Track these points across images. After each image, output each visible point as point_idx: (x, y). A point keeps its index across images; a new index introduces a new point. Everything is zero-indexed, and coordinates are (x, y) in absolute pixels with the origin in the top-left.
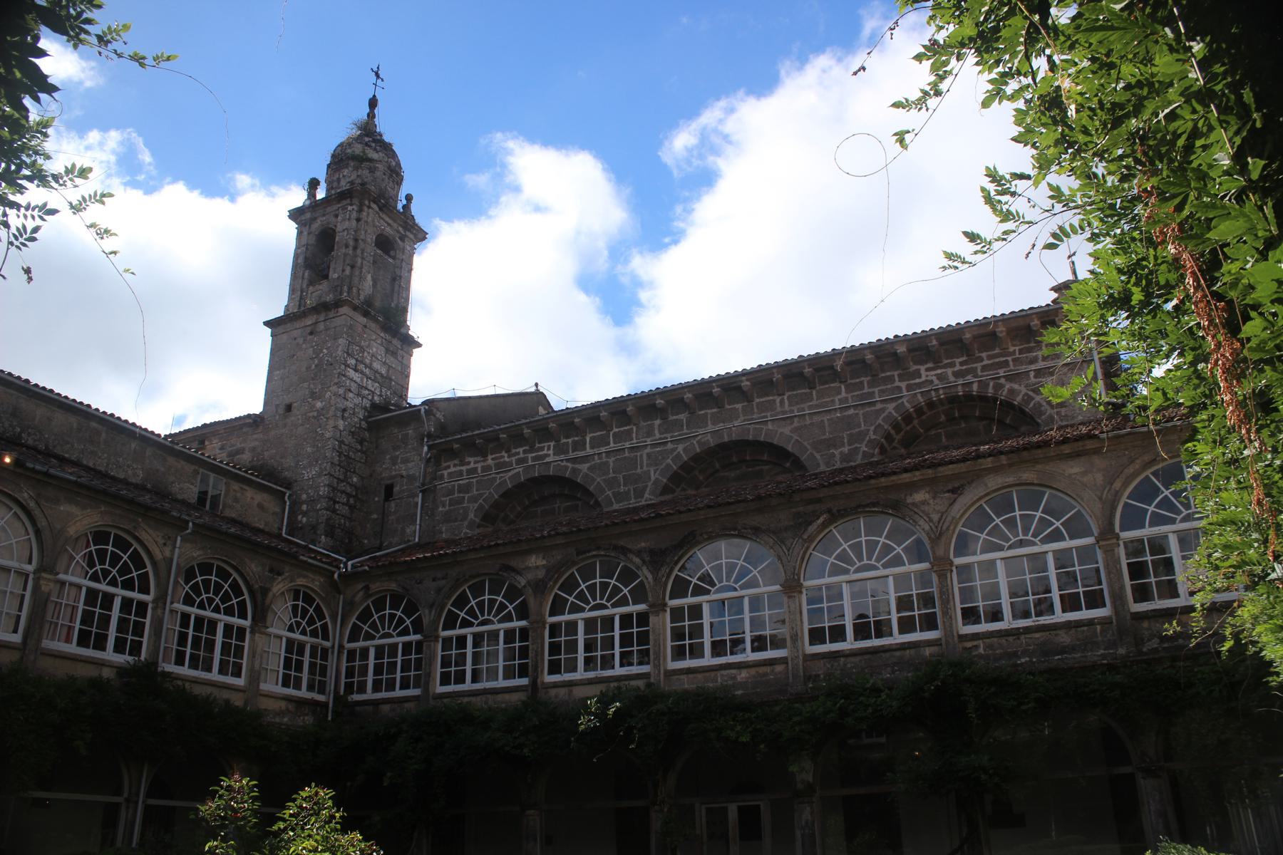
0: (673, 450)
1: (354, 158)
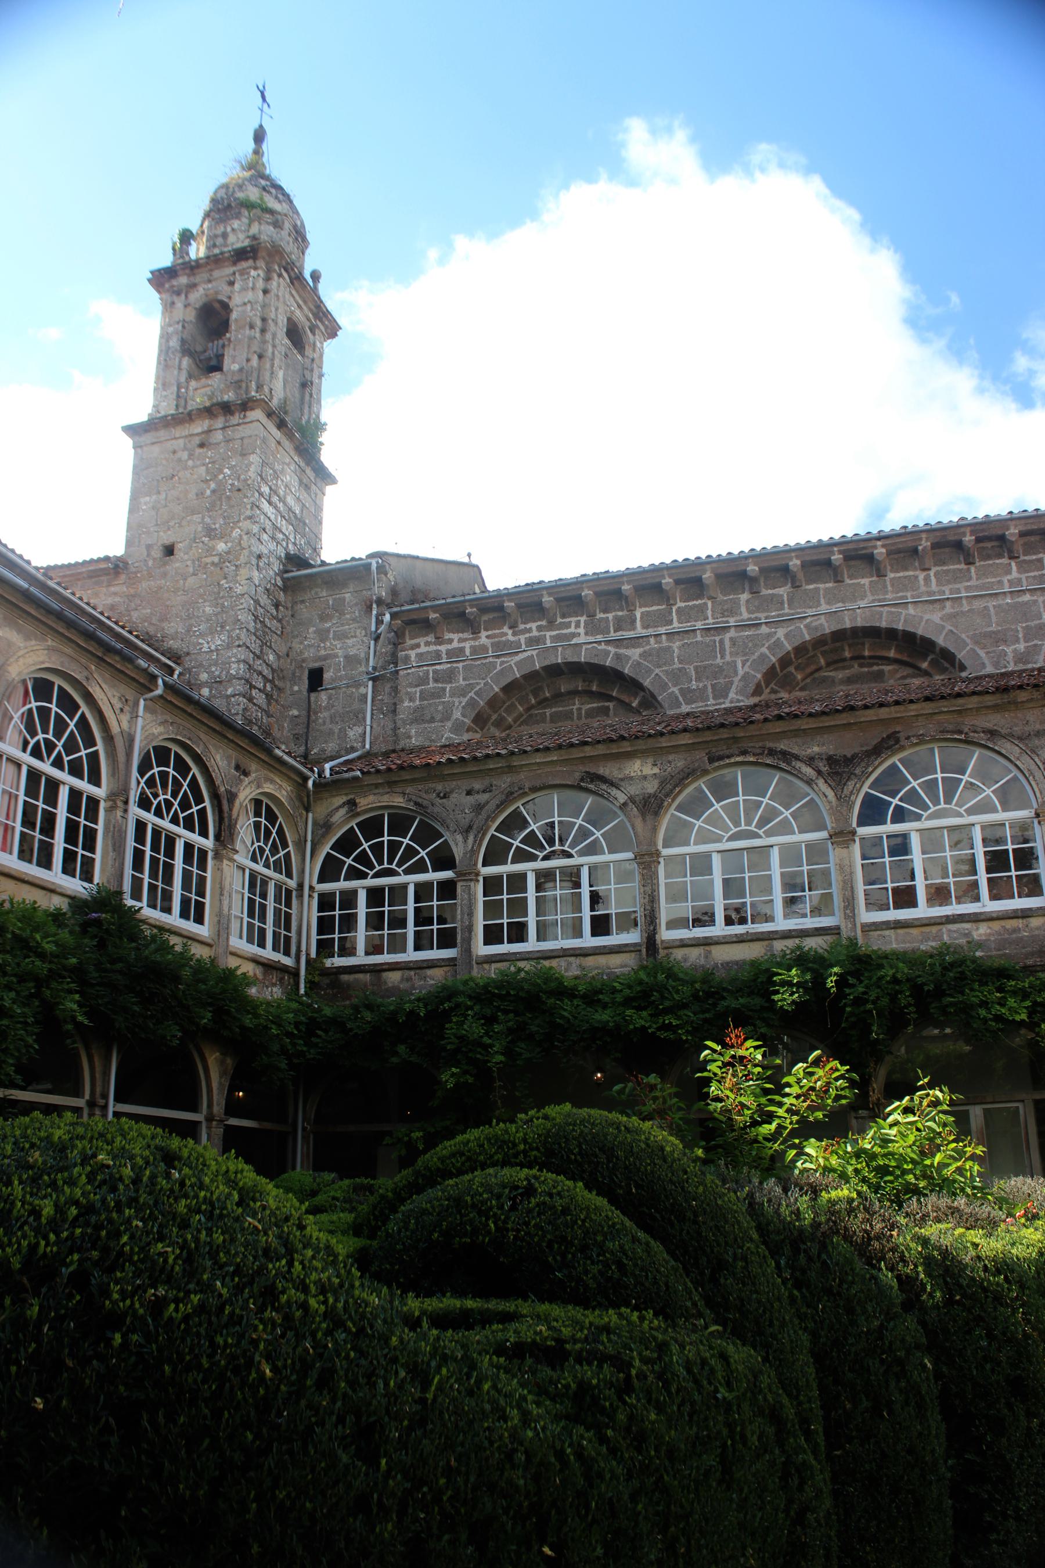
0: (769, 636)
1: (248, 205)
